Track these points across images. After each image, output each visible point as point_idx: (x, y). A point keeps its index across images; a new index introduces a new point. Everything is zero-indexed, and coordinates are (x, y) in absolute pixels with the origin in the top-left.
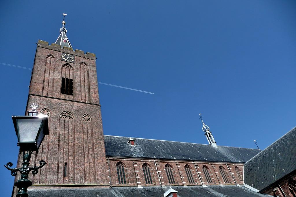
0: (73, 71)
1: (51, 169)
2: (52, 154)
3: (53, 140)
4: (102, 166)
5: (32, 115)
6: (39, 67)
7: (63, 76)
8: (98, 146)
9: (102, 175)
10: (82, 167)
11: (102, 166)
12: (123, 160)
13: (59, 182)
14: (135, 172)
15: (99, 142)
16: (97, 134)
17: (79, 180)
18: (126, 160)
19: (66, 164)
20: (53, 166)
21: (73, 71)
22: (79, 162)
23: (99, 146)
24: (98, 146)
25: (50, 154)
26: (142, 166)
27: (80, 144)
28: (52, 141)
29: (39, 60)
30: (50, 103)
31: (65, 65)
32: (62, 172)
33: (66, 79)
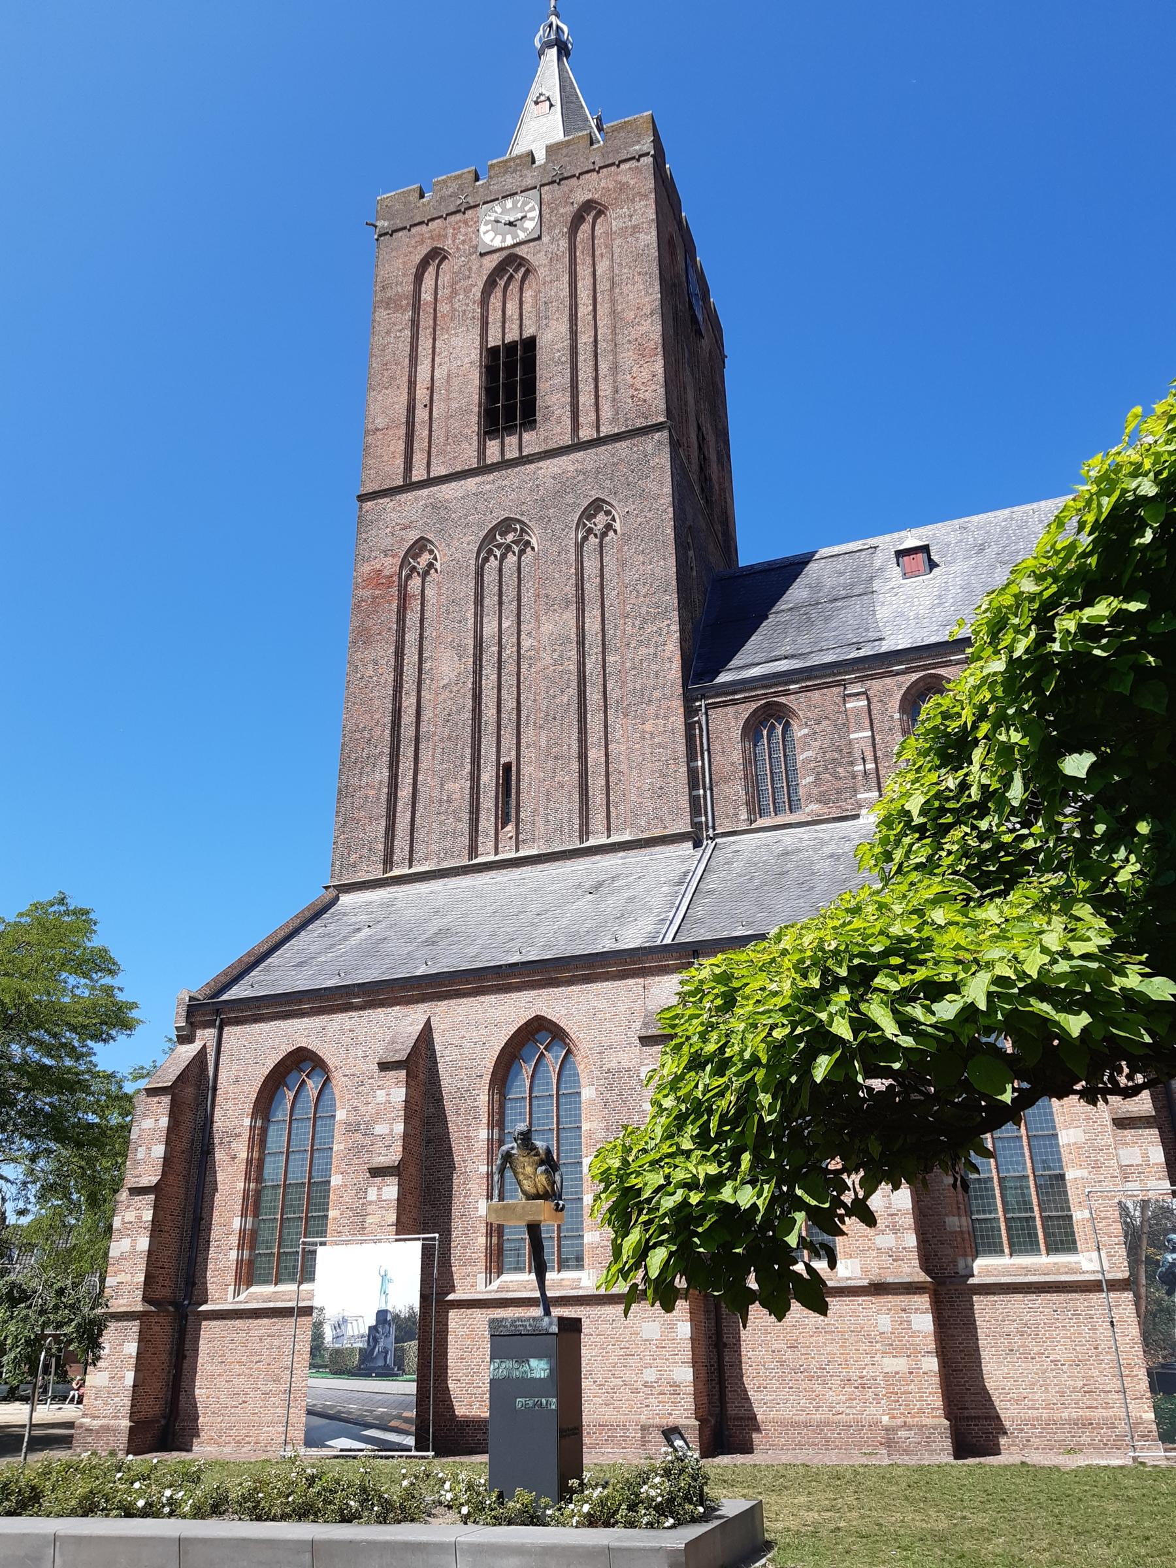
0: (883, 889)
1: (448, 801)
2: (450, 739)
3: (452, 675)
4: (659, 746)
5: (609, 836)
6: (389, 343)
7: (494, 340)
8: (646, 651)
9: (661, 788)
10: (569, 772)
11: (659, 746)
12: (786, 693)
13: (481, 850)
14: (850, 741)
15: (652, 628)
16: (643, 591)
17: (556, 830)
18: (803, 690)
19: (507, 767)
20: (452, 786)
21: (883, 889)
22: (556, 751)
23: (652, 651)
24: (646, 651)
25: (442, 740)
26: (899, 697)
27: (562, 665)
28: (446, 682)
29: (388, 307)
30: (435, 506)
31: (500, 270)
32: (492, 805)
33: (1102, 1291)
